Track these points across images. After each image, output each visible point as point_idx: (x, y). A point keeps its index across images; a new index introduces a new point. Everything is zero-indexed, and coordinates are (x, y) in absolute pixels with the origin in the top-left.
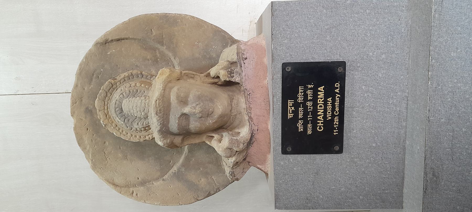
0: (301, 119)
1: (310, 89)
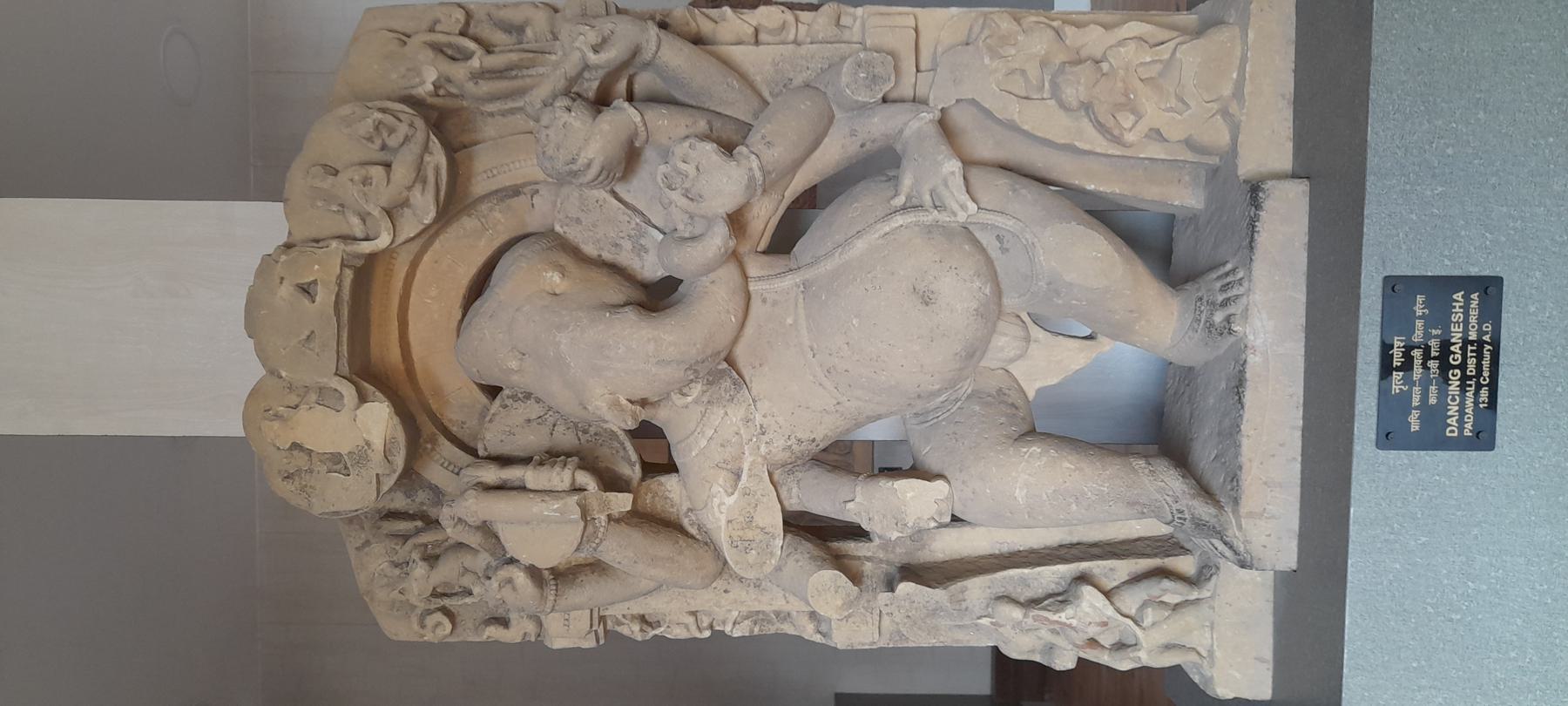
1: (1436, 337)
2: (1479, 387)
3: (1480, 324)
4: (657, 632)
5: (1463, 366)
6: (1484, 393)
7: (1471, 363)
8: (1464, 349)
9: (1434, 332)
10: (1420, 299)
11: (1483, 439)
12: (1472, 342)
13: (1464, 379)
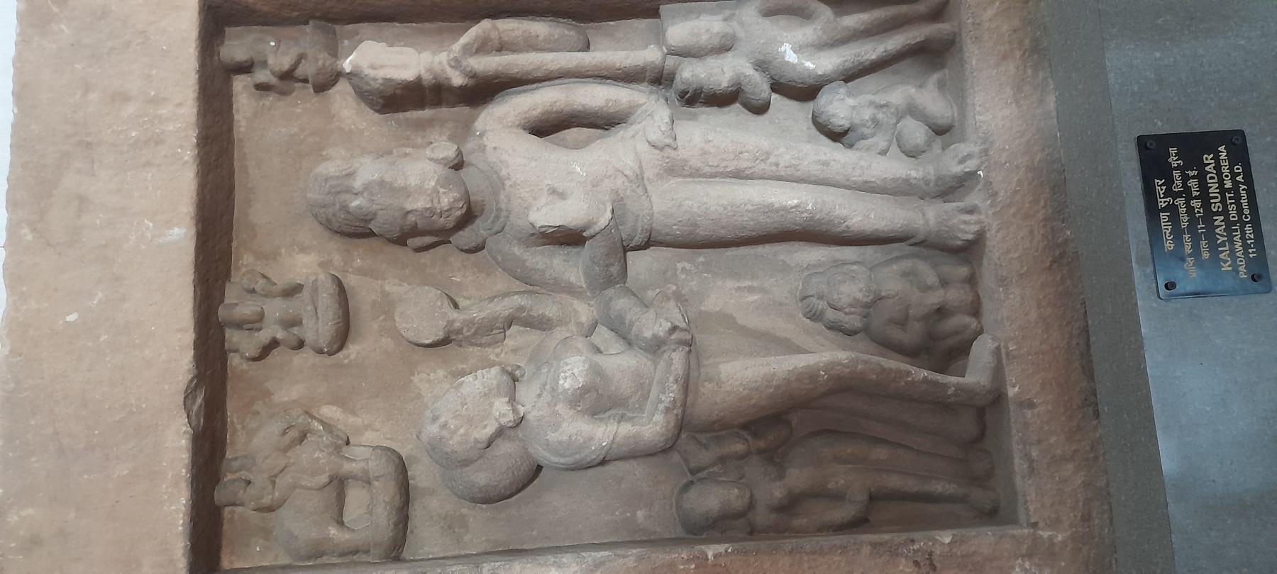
1: (1194, 177)
2: (1243, 224)
3: (1232, 171)
4: (737, 285)
5: (1225, 212)
6: (1249, 229)
7: (1232, 209)
8: (1223, 201)
9: (1191, 173)
10: (1173, 151)
11: (1236, 144)
12: (1229, 190)
13: (1229, 224)
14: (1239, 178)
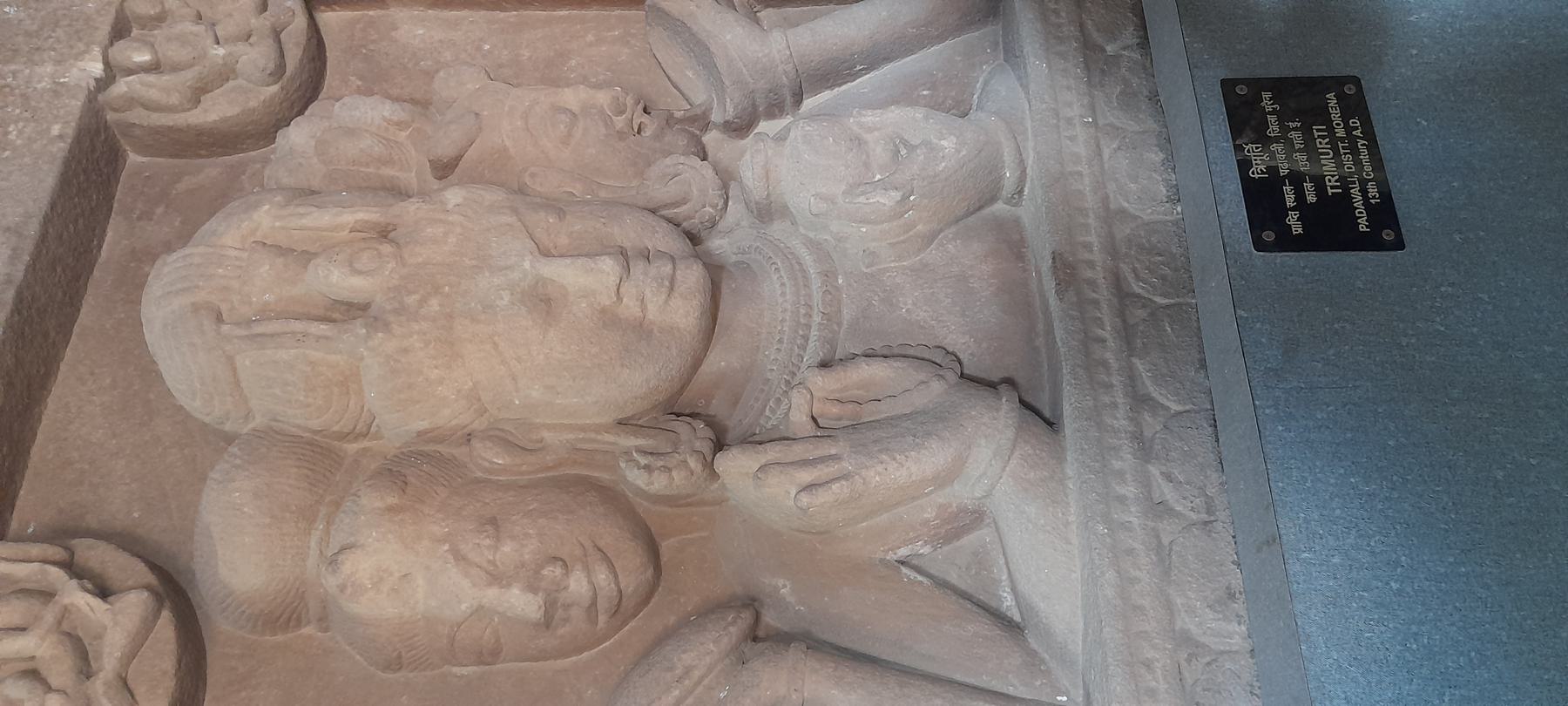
0: (1293, 209)
1: (1295, 129)
12: (1342, 140)
14: (1357, 133)
